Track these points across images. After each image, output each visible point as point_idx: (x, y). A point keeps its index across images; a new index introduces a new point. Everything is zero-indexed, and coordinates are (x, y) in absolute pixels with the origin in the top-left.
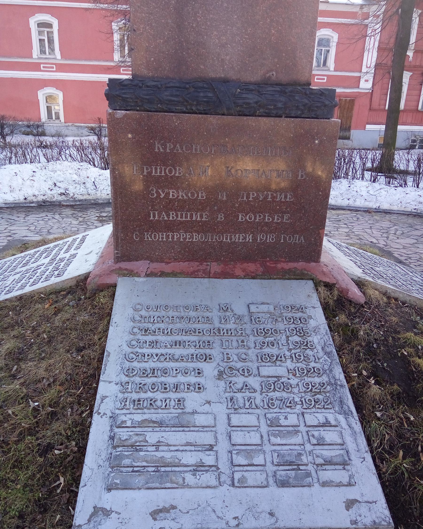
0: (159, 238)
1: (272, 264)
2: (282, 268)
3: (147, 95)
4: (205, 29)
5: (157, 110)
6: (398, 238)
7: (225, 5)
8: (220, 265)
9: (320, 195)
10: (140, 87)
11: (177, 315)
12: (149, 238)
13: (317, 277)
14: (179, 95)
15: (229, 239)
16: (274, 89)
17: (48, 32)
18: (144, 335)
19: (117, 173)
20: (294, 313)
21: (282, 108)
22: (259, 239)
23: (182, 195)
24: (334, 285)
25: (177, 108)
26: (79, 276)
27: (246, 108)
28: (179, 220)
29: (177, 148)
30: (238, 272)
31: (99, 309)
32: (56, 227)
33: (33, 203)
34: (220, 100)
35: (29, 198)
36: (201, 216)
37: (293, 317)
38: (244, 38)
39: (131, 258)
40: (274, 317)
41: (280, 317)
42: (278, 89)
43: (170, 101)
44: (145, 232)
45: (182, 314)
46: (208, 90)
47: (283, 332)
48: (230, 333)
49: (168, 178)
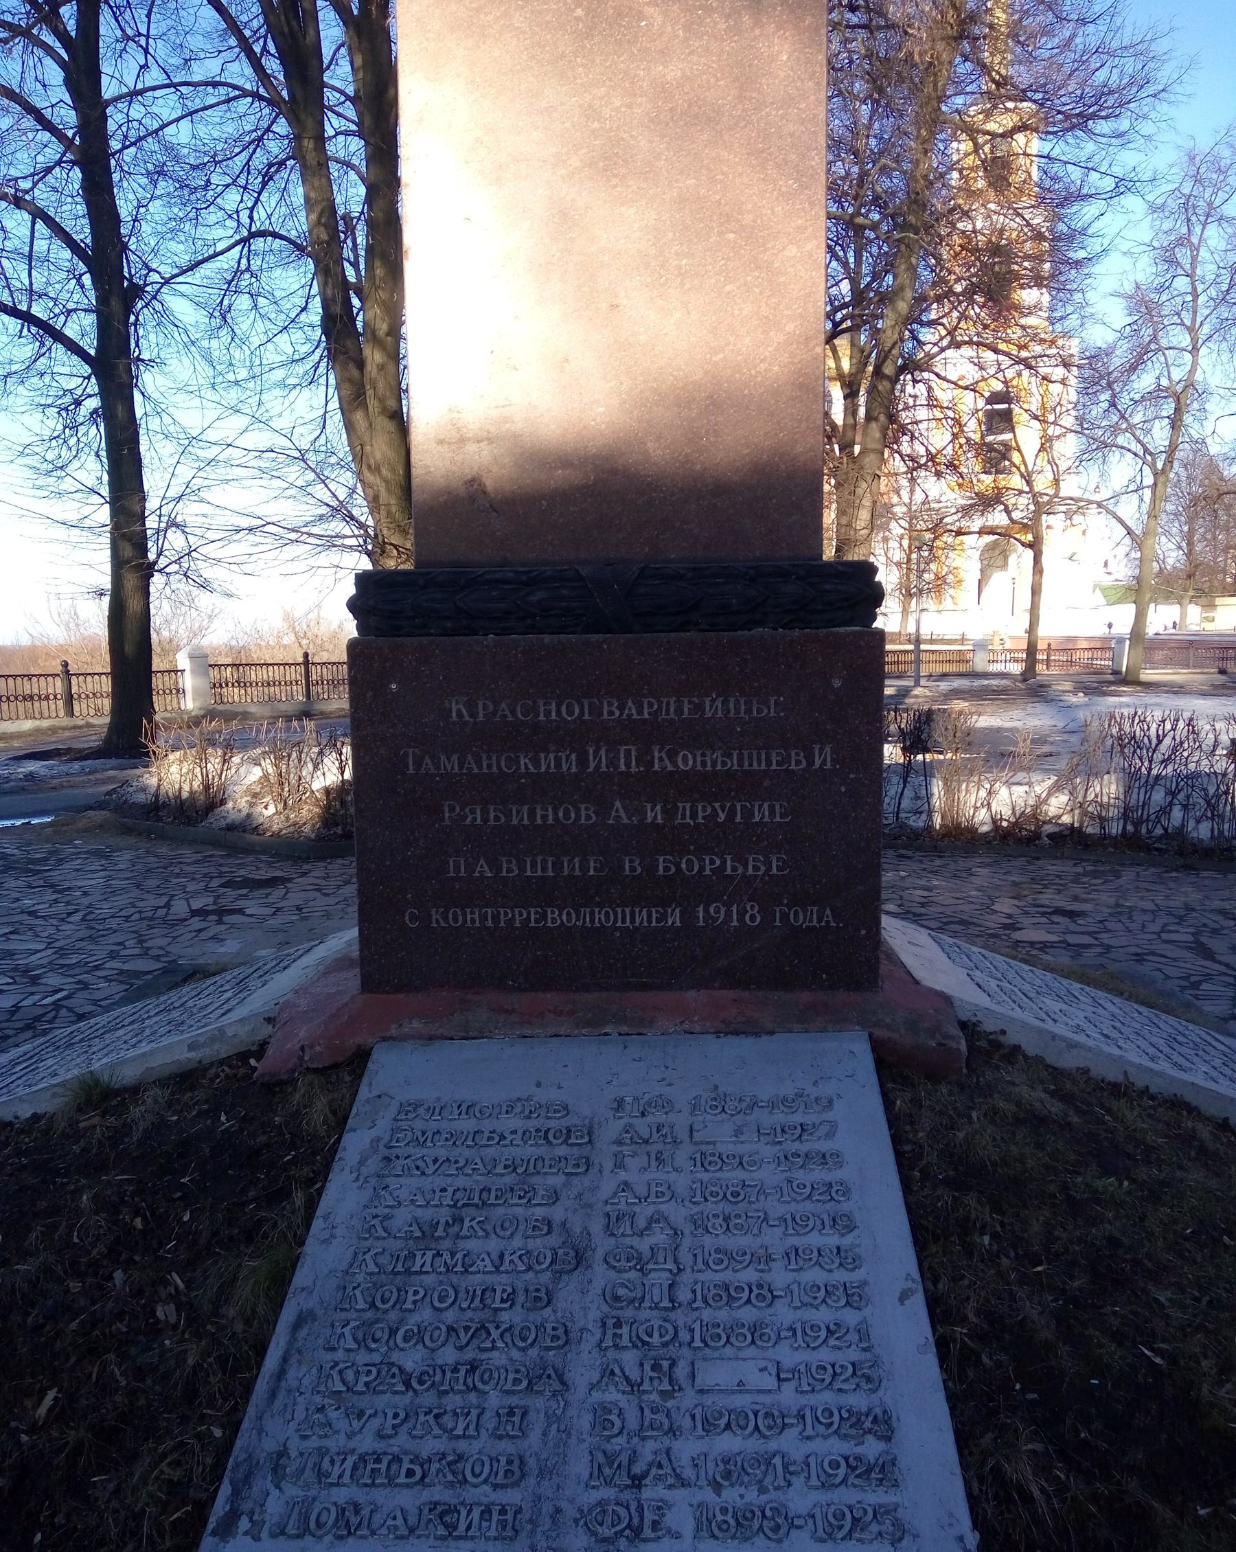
0: (695, 761)
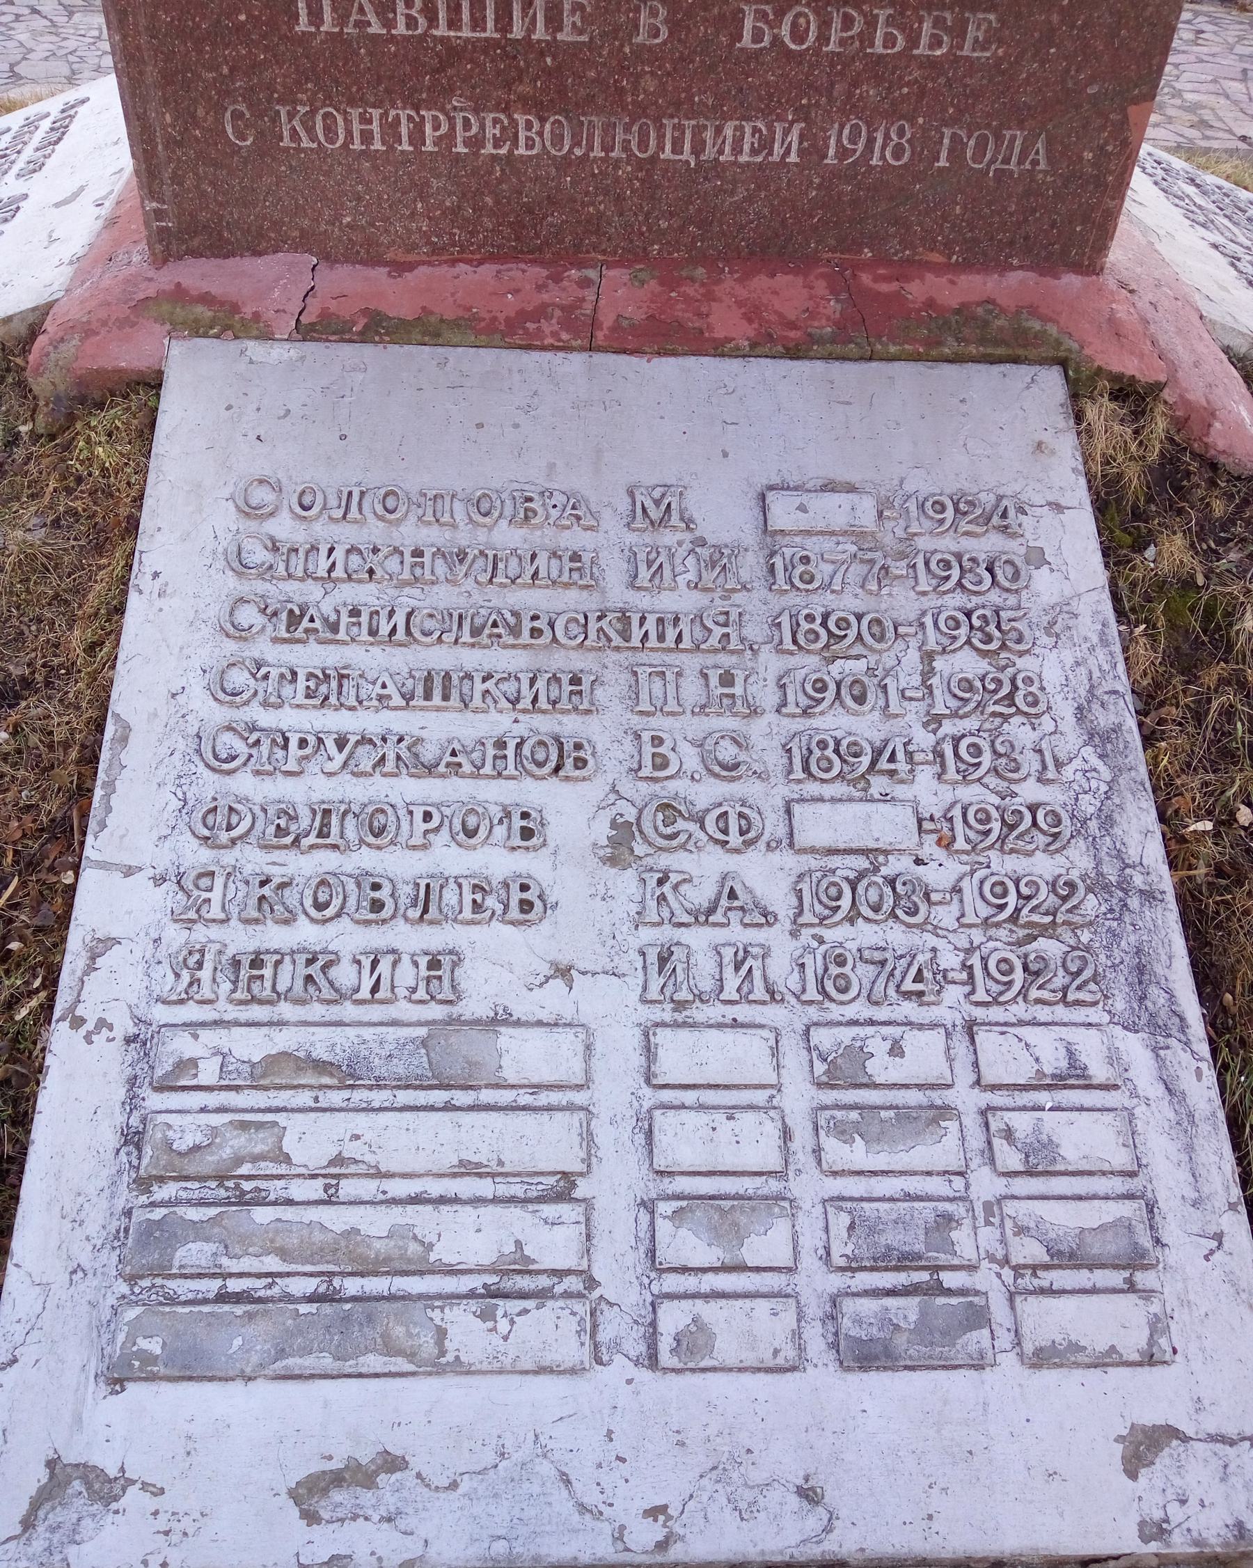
0: (349, 133)
1: (887, 279)
2: (930, 303)
8: (642, 283)
11: (440, 542)
12: (302, 134)
13: (1087, 351)
15: (687, 147)
18: (285, 641)
20: (967, 533)
22: (831, 152)
24: (1157, 388)
28: (442, 40)
31: (92, 493)
32: (42, 49)
37: (959, 557)
39: (228, 242)
41: (902, 556)
44: (279, 101)
45: (463, 537)
48: (671, 634)
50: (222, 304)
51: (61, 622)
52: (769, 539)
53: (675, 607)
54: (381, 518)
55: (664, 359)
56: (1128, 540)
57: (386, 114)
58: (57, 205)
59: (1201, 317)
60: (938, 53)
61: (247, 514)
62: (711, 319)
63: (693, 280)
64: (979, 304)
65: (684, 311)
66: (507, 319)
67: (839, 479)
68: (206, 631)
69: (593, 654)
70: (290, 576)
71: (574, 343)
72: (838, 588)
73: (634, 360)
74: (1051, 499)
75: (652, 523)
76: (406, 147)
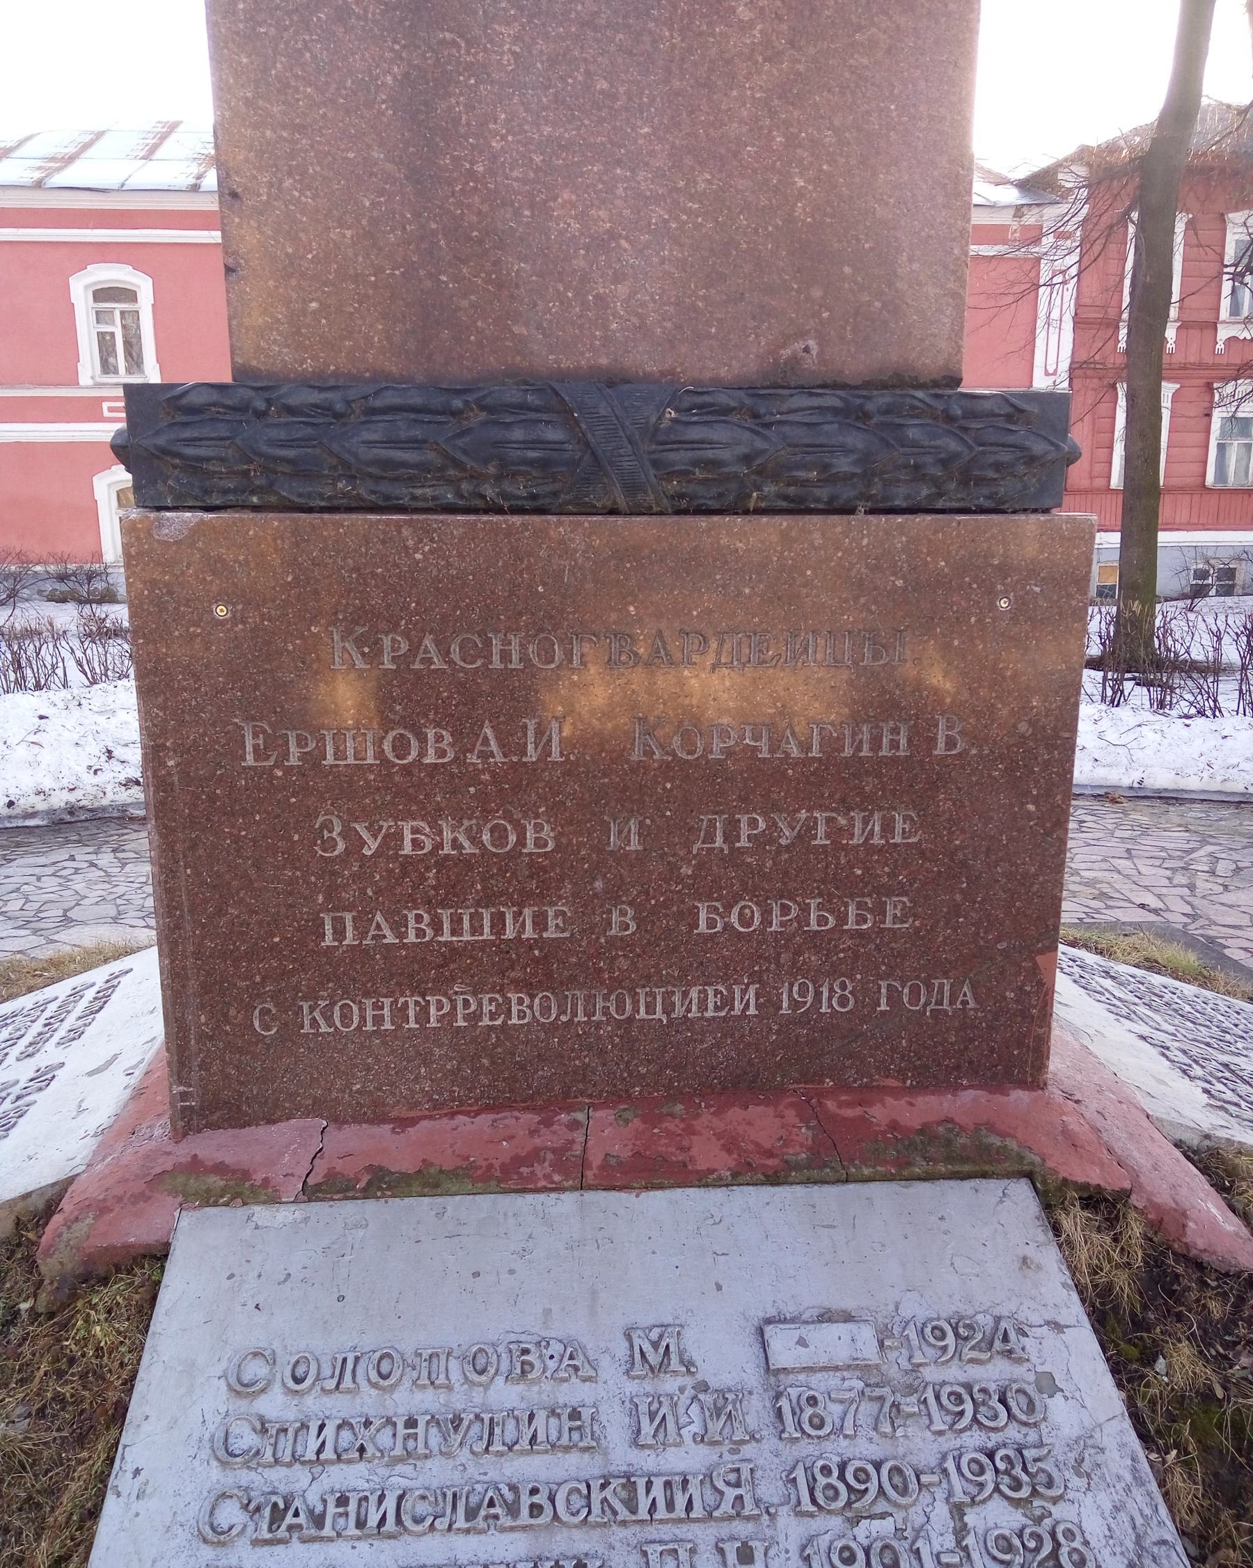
0: (363, 1019)
1: (849, 1104)
2: (894, 1126)
3: (283, 444)
4: (524, 181)
5: (336, 503)
6: (1226, 887)
7: (602, 85)
8: (627, 1121)
9: (1029, 816)
10: (261, 415)
11: (434, 1408)
12: (322, 1022)
13: (1049, 1164)
14: (425, 441)
15: (659, 1008)
16: (816, 402)
17: (122, 313)
18: (267, 1542)
19: (171, 763)
20: (971, 1361)
21: (854, 475)
22: (785, 1005)
23: (455, 840)
24: (1124, 1195)
25: (419, 492)
26: (27, 1195)
27: (704, 482)
28: (446, 944)
29: (426, 651)
30: (706, 1153)
31: (83, 1376)
32: (94, 896)
33: (33, 815)
34: (593, 454)
35: (22, 801)
36: (540, 922)
37: (968, 1387)
38: (685, 211)
39: (246, 1114)
40: (886, 1391)
41: (911, 1390)
42: (837, 403)
43: (387, 464)
44: (302, 999)
45: (458, 1401)
46: (545, 417)
47: (935, 1478)
48: (680, 1501)
49: (390, 775)
50: (234, 1172)
51: (29, 1533)
52: (772, 1379)
53: (681, 1466)
54: (375, 1385)
55: (651, 1193)
56: (1134, 1352)
57: (396, 1001)
58: (91, 1074)
59: (1148, 1117)
60: (865, 927)
61: (238, 1393)
62: (694, 1152)
63: (672, 1115)
64: (939, 1123)
65: (667, 1145)
66: (503, 1165)
67: (834, 1307)
68: (183, 1535)
69: (598, 1532)
70: (276, 1461)
71: (566, 1184)
72: (850, 1432)
73: (623, 1195)
74: (1048, 1318)
75: (652, 1368)
76: (413, 1025)
